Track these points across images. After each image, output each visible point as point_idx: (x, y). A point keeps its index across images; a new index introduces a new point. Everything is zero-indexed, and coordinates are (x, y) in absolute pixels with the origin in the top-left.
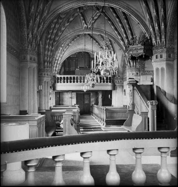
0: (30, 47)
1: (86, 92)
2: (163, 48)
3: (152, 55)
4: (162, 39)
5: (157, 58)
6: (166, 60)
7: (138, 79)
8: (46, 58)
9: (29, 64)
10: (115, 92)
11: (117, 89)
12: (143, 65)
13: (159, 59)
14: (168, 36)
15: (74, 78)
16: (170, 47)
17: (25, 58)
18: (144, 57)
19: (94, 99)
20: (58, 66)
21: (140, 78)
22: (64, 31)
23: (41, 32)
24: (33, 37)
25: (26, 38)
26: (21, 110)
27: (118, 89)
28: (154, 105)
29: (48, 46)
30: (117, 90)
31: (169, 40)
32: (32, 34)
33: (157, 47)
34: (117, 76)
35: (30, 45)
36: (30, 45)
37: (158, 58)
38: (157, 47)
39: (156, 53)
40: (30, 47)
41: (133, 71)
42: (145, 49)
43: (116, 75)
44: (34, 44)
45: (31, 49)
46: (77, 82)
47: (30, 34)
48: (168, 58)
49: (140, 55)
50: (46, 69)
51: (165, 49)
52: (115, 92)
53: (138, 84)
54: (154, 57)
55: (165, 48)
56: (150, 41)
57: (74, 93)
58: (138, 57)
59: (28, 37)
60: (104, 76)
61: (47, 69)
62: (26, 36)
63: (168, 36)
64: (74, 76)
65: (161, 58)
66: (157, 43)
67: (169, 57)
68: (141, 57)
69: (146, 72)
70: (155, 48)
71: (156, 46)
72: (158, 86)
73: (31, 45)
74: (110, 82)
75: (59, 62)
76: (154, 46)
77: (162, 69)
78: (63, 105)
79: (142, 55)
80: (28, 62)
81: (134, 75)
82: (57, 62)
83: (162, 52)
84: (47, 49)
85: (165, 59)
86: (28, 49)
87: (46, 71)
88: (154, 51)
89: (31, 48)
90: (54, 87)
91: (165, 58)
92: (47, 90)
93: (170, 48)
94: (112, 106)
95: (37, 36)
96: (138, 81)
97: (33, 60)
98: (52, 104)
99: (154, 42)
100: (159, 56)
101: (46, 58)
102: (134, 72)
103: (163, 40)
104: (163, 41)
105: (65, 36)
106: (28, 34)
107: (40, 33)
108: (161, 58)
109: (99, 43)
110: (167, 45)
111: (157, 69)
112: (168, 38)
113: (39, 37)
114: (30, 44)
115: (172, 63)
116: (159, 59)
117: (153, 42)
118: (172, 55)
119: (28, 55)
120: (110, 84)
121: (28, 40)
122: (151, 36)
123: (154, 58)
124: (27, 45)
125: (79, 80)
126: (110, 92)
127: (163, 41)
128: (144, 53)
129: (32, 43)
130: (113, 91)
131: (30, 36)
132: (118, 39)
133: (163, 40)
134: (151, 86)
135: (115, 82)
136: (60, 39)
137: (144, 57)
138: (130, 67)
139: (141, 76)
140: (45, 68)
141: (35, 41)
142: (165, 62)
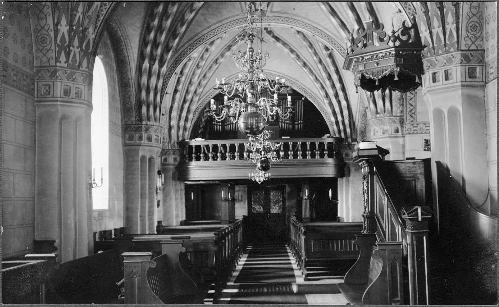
0: (63, 58)
1: (262, 183)
2: (452, 50)
3: (421, 71)
4: (447, 26)
5: (434, 81)
6: (462, 86)
7: (399, 144)
8: (144, 94)
9: (59, 107)
10: (344, 185)
11: (349, 175)
12: (412, 108)
13: (441, 83)
14: (465, 15)
15: (233, 147)
16: (473, 47)
17: (49, 89)
18: (396, 79)
19: (295, 200)
20: (191, 116)
21: (404, 141)
22: (194, 22)
23: (98, 16)
24: (70, 31)
25: (52, 34)
26: (38, 239)
27: (351, 174)
28: (420, 219)
29: (149, 63)
30: (351, 178)
31: (467, 28)
32: (70, 24)
33: (434, 48)
34: (350, 140)
35: (63, 54)
36: (63, 54)
37: (439, 81)
38: (434, 48)
39: (432, 65)
40: (63, 58)
41: (383, 123)
42: (401, 56)
43: (346, 137)
44: (75, 50)
45: (66, 65)
46: (224, 158)
47: (64, 22)
48: (468, 79)
49: (387, 73)
50: (144, 123)
51: (458, 55)
52: (344, 185)
53: (387, 158)
54: (427, 78)
55: (458, 49)
56: (412, 32)
57: (241, 186)
58: (379, 80)
59: (56, 32)
60: (248, 131)
61: (147, 124)
62: (52, 27)
63: (464, 18)
64: (223, 142)
65: (446, 80)
66: (434, 38)
67: (471, 74)
68: (387, 83)
69: (421, 125)
70: (429, 51)
71: (431, 46)
72: (441, 161)
73: (68, 55)
74: (330, 156)
75: (193, 108)
76: (425, 46)
77: (453, 112)
78: (212, 217)
79: (391, 76)
80: (57, 101)
81: (386, 135)
82: (189, 108)
83: (449, 61)
84: (146, 68)
85: (460, 84)
86: (58, 64)
87: (144, 129)
88: (425, 63)
89: (67, 62)
90: (181, 173)
91: (459, 80)
92: (141, 179)
93: (472, 50)
94: (339, 221)
95: (86, 29)
96: (385, 147)
97: (73, 94)
98: (177, 216)
99: (424, 34)
100: (441, 76)
101: (144, 94)
102: (387, 127)
103: (451, 26)
104: (451, 31)
105: (196, 35)
106: (56, 25)
107: (93, 20)
108: (446, 80)
109: (298, 56)
110: (463, 43)
111: (438, 113)
112: (463, 23)
113: (91, 30)
114: (65, 50)
115: (482, 95)
116: (441, 83)
117: (421, 35)
118: (478, 69)
119: (59, 84)
120: (331, 161)
121: (56, 41)
122: (414, 18)
123: (427, 81)
124: (53, 55)
125: (236, 154)
126: (332, 183)
127: (451, 31)
128: (397, 66)
129: (69, 46)
130: (339, 179)
131: (64, 28)
132: (342, 39)
133: (451, 26)
134: (427, 162)
135: (344, 156)
136: (181, 44)
137: (396, 79)
138: (377, 113)
139: (408, 138)
140: (141, 120)
141: (81, 43)
142: (460, 92)
